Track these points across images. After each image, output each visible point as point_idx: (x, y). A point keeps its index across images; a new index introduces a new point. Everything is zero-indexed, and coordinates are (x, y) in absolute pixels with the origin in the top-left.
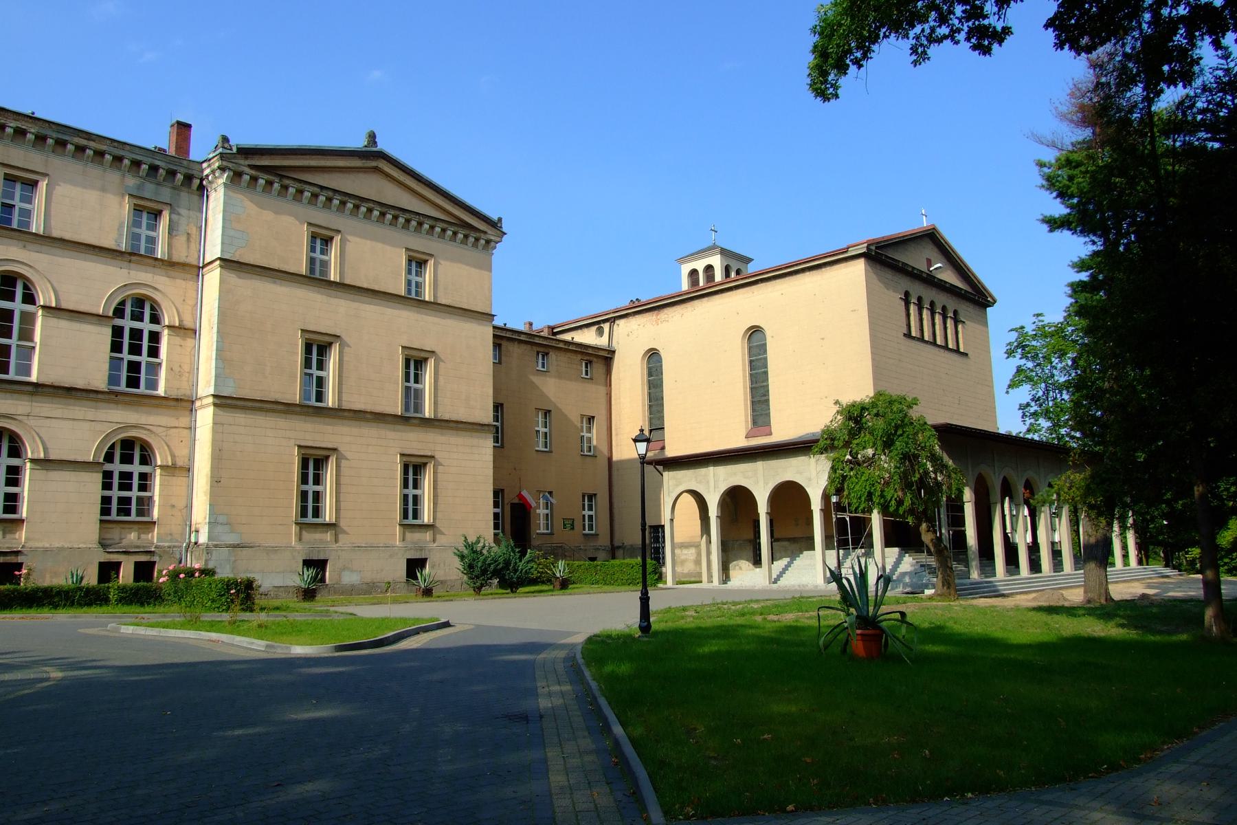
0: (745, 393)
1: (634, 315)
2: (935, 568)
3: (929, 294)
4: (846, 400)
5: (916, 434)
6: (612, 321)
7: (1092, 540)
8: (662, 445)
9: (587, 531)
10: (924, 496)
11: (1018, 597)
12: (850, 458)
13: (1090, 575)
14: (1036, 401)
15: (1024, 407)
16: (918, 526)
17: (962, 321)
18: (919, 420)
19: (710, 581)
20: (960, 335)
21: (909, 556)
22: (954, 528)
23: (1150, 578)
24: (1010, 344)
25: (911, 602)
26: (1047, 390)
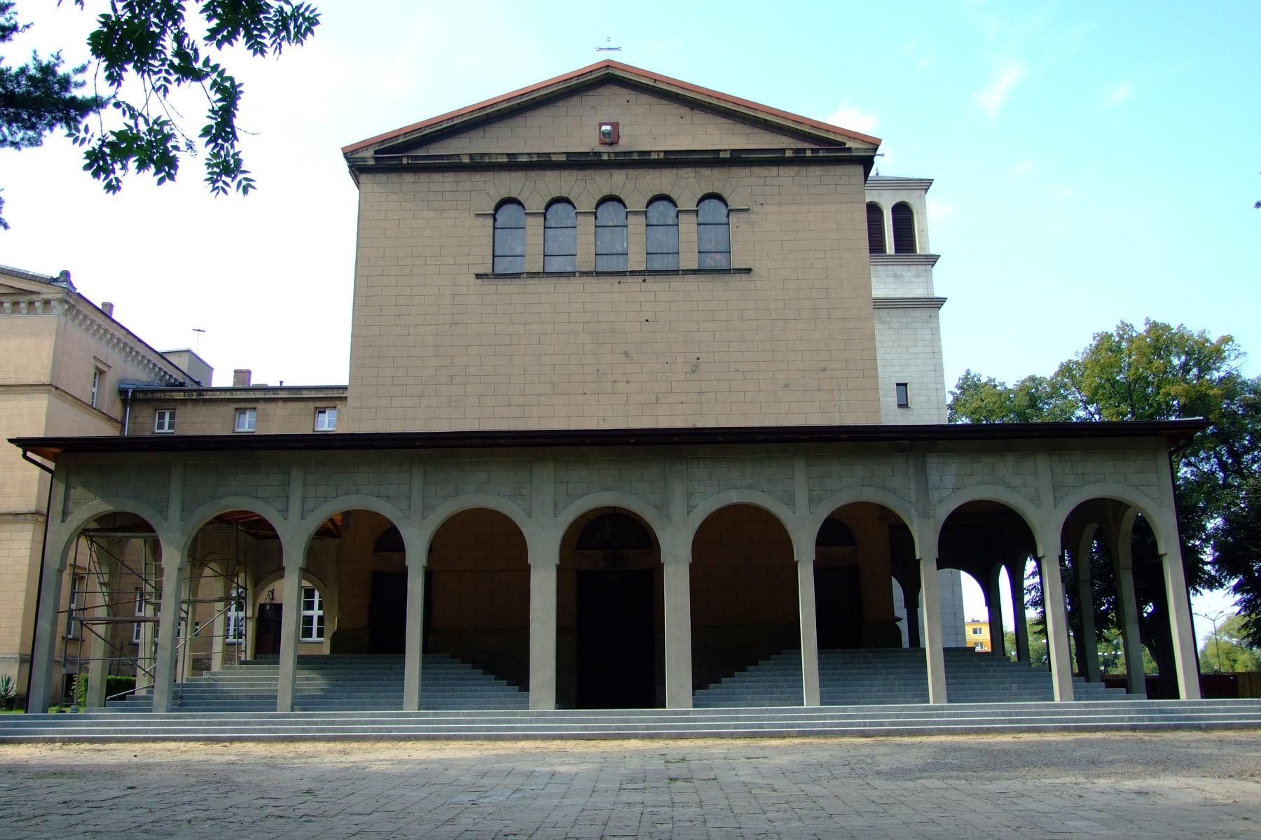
9: (231, 640)
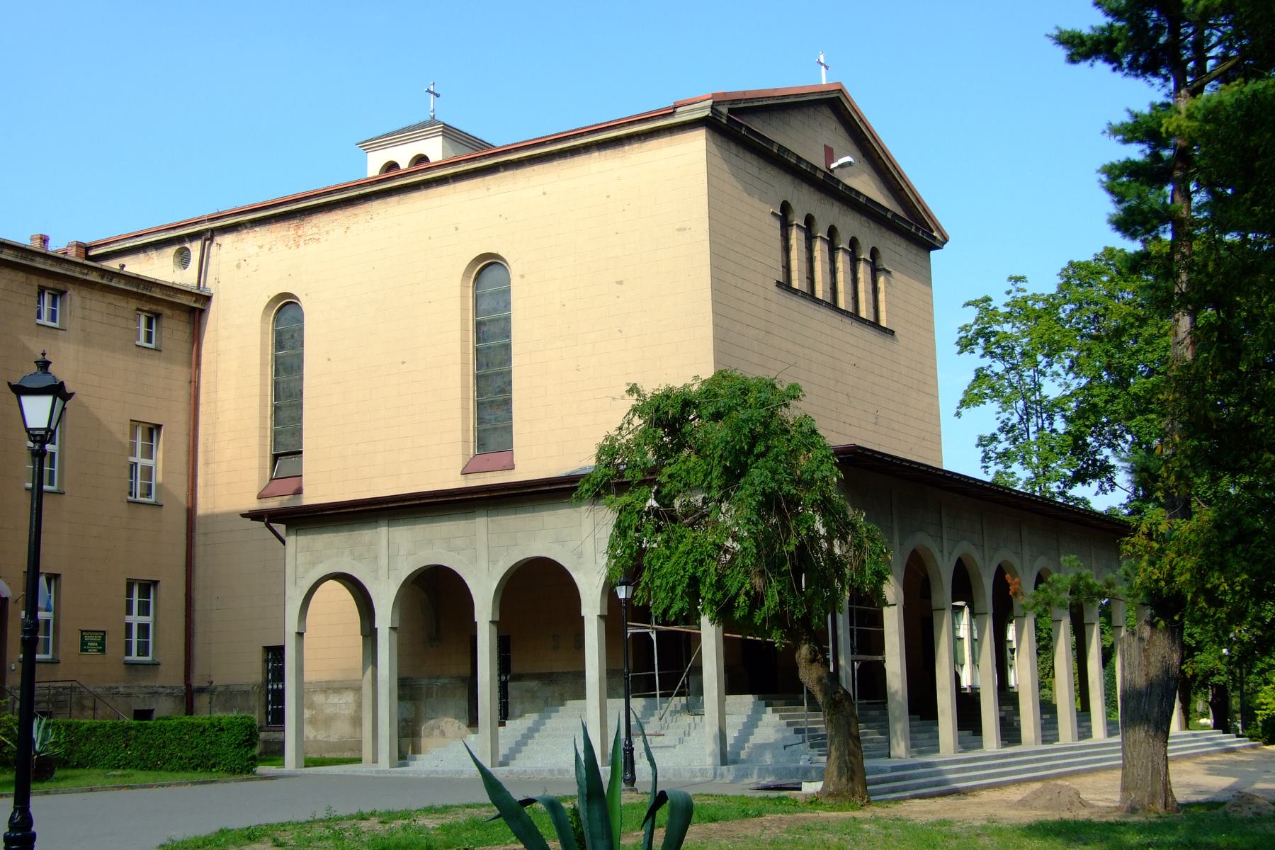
0: (464, 387)
1: (252, 227)
2: (824, 737)
3: (828, 213)
4: (652, 385)
5: (793, 453)
6: (208, 236)
7: (1141, 682)
8: (295, 487)
9: (134, 657)
10: (807, 587)
11: (986, 795)
12: (655, 504)
13: (1135, 754)
14: (1008, 432)
15: (984, 442)
16: (791, 651)
17: (884, 269)
18: (801, 425)
19: (375, 761)
20: (882, 296)
21: (774, 711)
22: (863, 657)
23: (1207, 754)
24: (965, 328)
25: (774, 812)
26: (1028, 414)
